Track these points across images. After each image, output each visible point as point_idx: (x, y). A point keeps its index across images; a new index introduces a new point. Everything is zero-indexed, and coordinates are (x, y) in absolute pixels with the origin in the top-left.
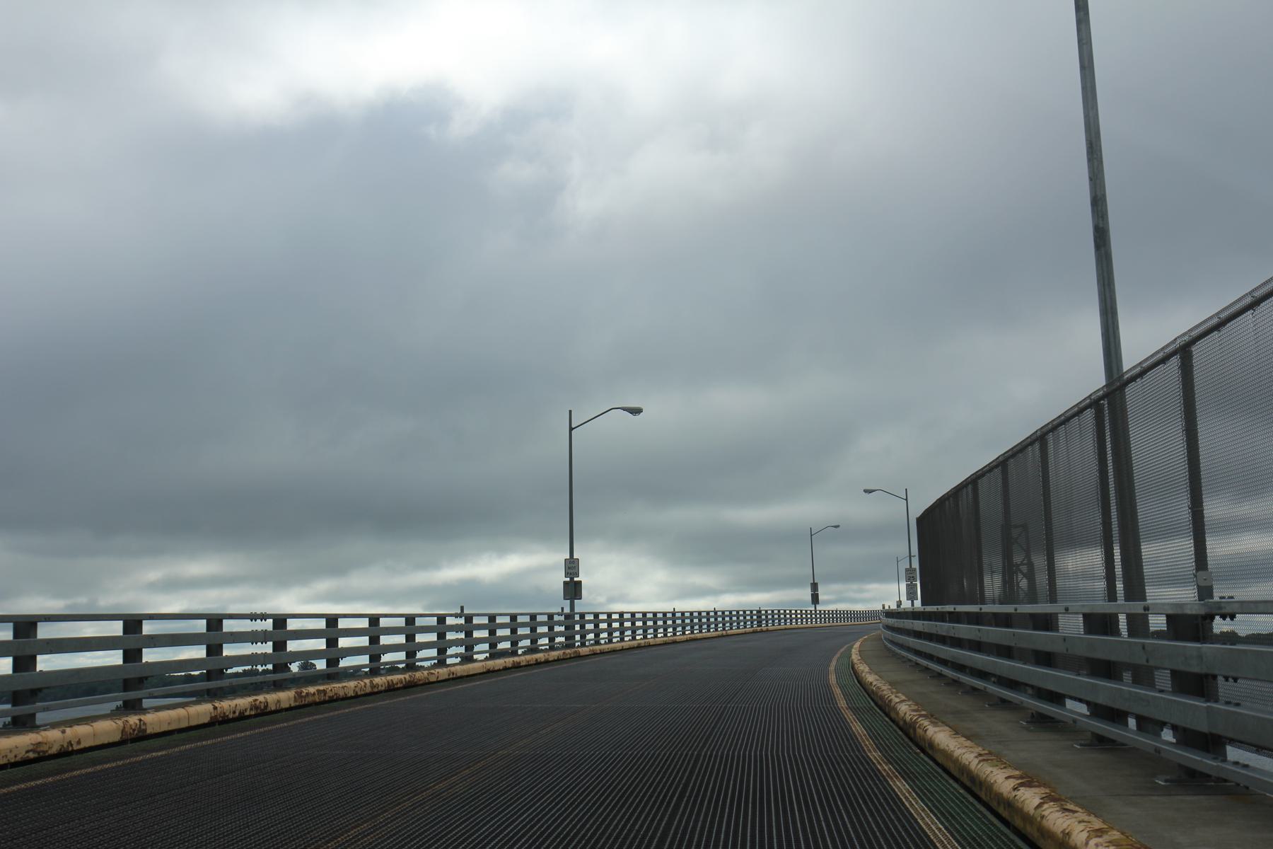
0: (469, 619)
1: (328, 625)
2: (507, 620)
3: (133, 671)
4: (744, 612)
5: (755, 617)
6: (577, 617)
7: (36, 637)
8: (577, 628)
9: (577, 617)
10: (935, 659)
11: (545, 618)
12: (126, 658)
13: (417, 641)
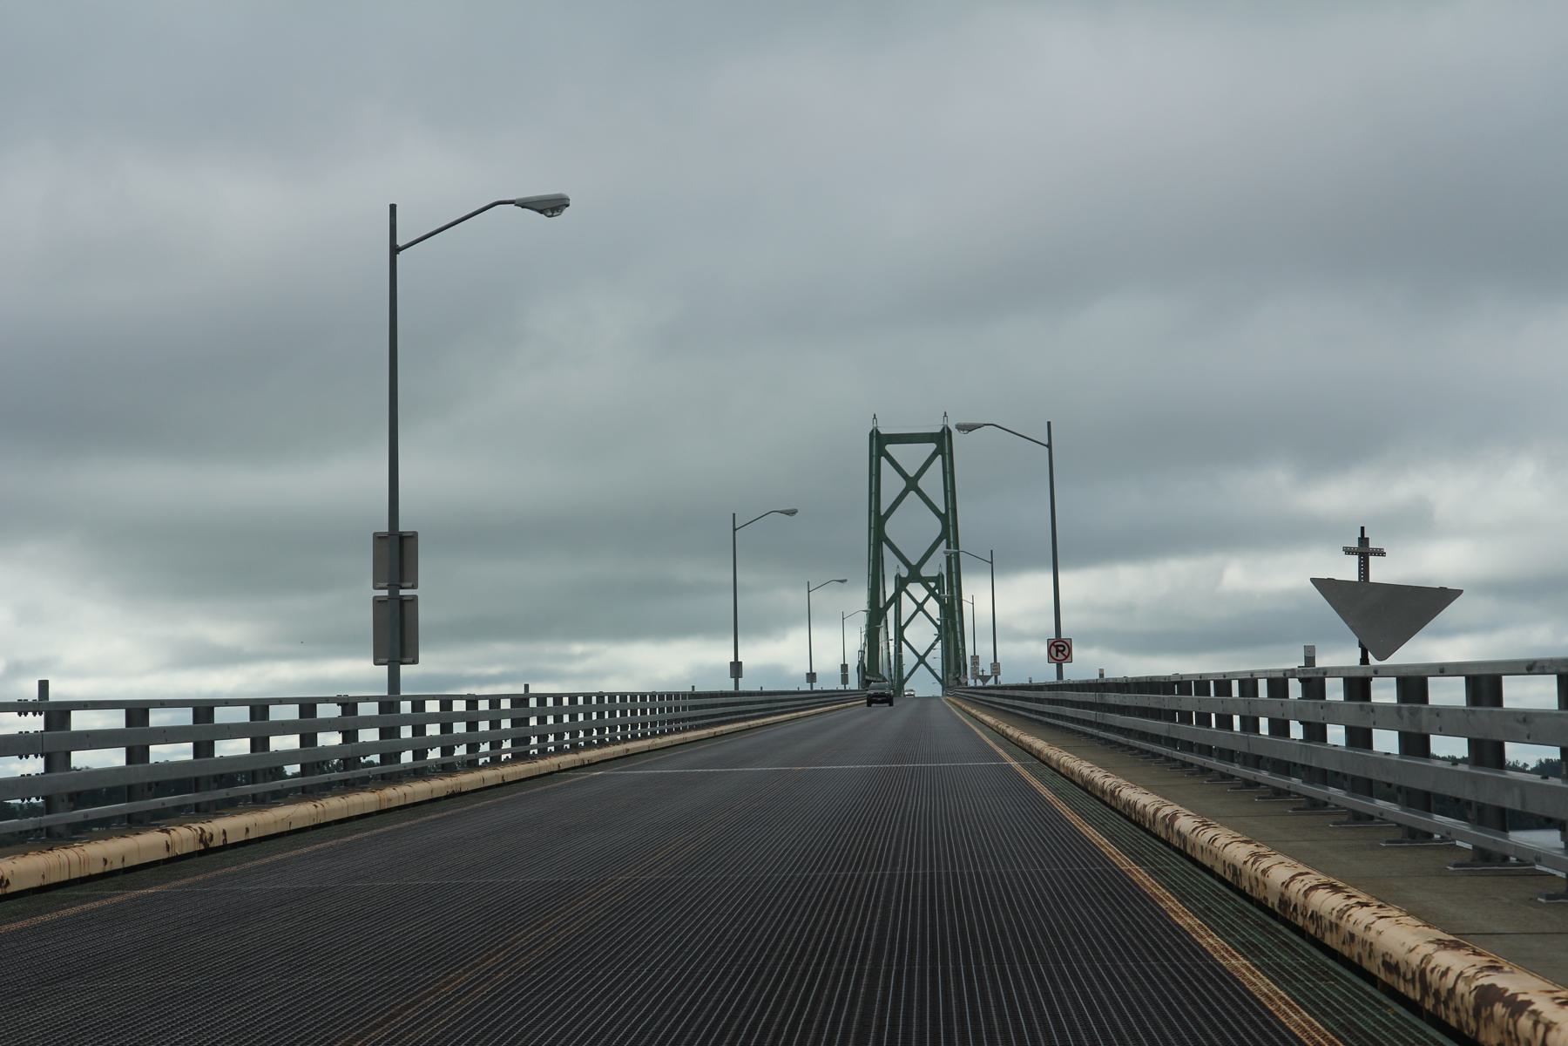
0: (58, 715)
1: (196, 718)
2: (242, 715)
3: (140, 775)
4: (446, 703)
5: (506, 724)
6: (406, 707)
7: (399, 712)
8: (406, 732)
9: (406, 707)
10: (1149, 738)
11: (291, 713)
12: (197, 752)
13: (319, 745)
